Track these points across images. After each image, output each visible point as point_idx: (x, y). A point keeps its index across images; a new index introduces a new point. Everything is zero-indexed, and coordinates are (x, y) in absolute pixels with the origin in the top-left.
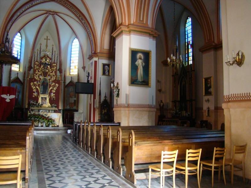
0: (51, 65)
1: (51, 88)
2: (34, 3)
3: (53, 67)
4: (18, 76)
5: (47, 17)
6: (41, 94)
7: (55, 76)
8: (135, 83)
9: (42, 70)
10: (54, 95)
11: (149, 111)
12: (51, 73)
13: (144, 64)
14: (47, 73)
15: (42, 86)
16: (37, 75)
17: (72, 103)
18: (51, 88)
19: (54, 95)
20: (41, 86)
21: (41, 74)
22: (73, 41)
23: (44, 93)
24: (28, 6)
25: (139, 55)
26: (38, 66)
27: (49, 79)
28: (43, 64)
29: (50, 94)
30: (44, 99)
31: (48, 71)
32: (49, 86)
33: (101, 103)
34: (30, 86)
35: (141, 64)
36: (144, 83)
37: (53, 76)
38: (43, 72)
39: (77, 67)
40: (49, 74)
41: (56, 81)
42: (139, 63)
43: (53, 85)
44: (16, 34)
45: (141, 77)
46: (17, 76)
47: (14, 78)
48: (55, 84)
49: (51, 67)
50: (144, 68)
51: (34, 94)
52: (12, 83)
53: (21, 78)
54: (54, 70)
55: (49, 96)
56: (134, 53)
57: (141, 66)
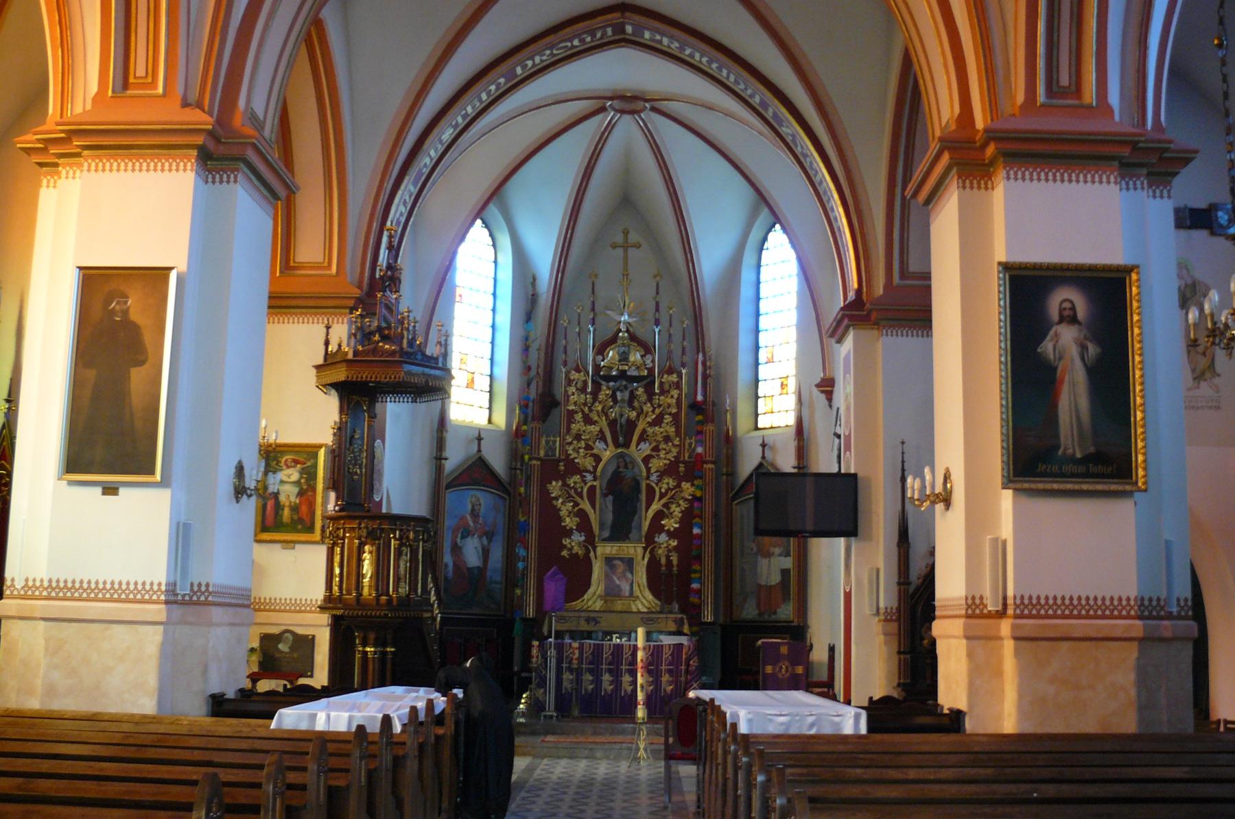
0: (648, 382)
1: (655, 506)
2: (519, 70)
3: (663, 392)
4: (479, 451)
5: (611, 127)
6: (604, 540)
7: (677, 442)
8: (1041, 467)
9: (604, 412)
10: (674, 543)
11: (1141, 640)
12: (651, 424)
13: (1093, 350)
14: (632, 425)
15: (611, 498)
16: (578, 437)
17: (770, 588)
18: (655, 506)
19: (674, 543)
20: (605, 495)
21: (601, 431)
22: (765, 239)
23: (620, 532)
24: (493, 88)
25: (1062, 297)
26: (583, 390)
27: (646, 460)
28: (608, 378)
29: (650, 541)
30: (621, 567)
31: (634, 414)
32: (643, 496)
33: (912, 588)
34: (546, 501)
35: (1074, 351)
36: (1100, 469)
37: (667, 439)
38: (612, 424)
39: (792, 385)
40: (644, 431)
41: (682, 468)
42: (1066, 344)
43: (668, 490)
44: (472, 223)
45: (1081, 436)
46: (476, 448)
47: (467, 459)
48: (679, 486)
49: (650, 394)
50: (1093, 371)
51: (566, 542)
52: (448, 486)
53: (497, 460)
54: (669, 406)
55: (645, 549)
56: (1027, 288)
57: (1078, 363)
